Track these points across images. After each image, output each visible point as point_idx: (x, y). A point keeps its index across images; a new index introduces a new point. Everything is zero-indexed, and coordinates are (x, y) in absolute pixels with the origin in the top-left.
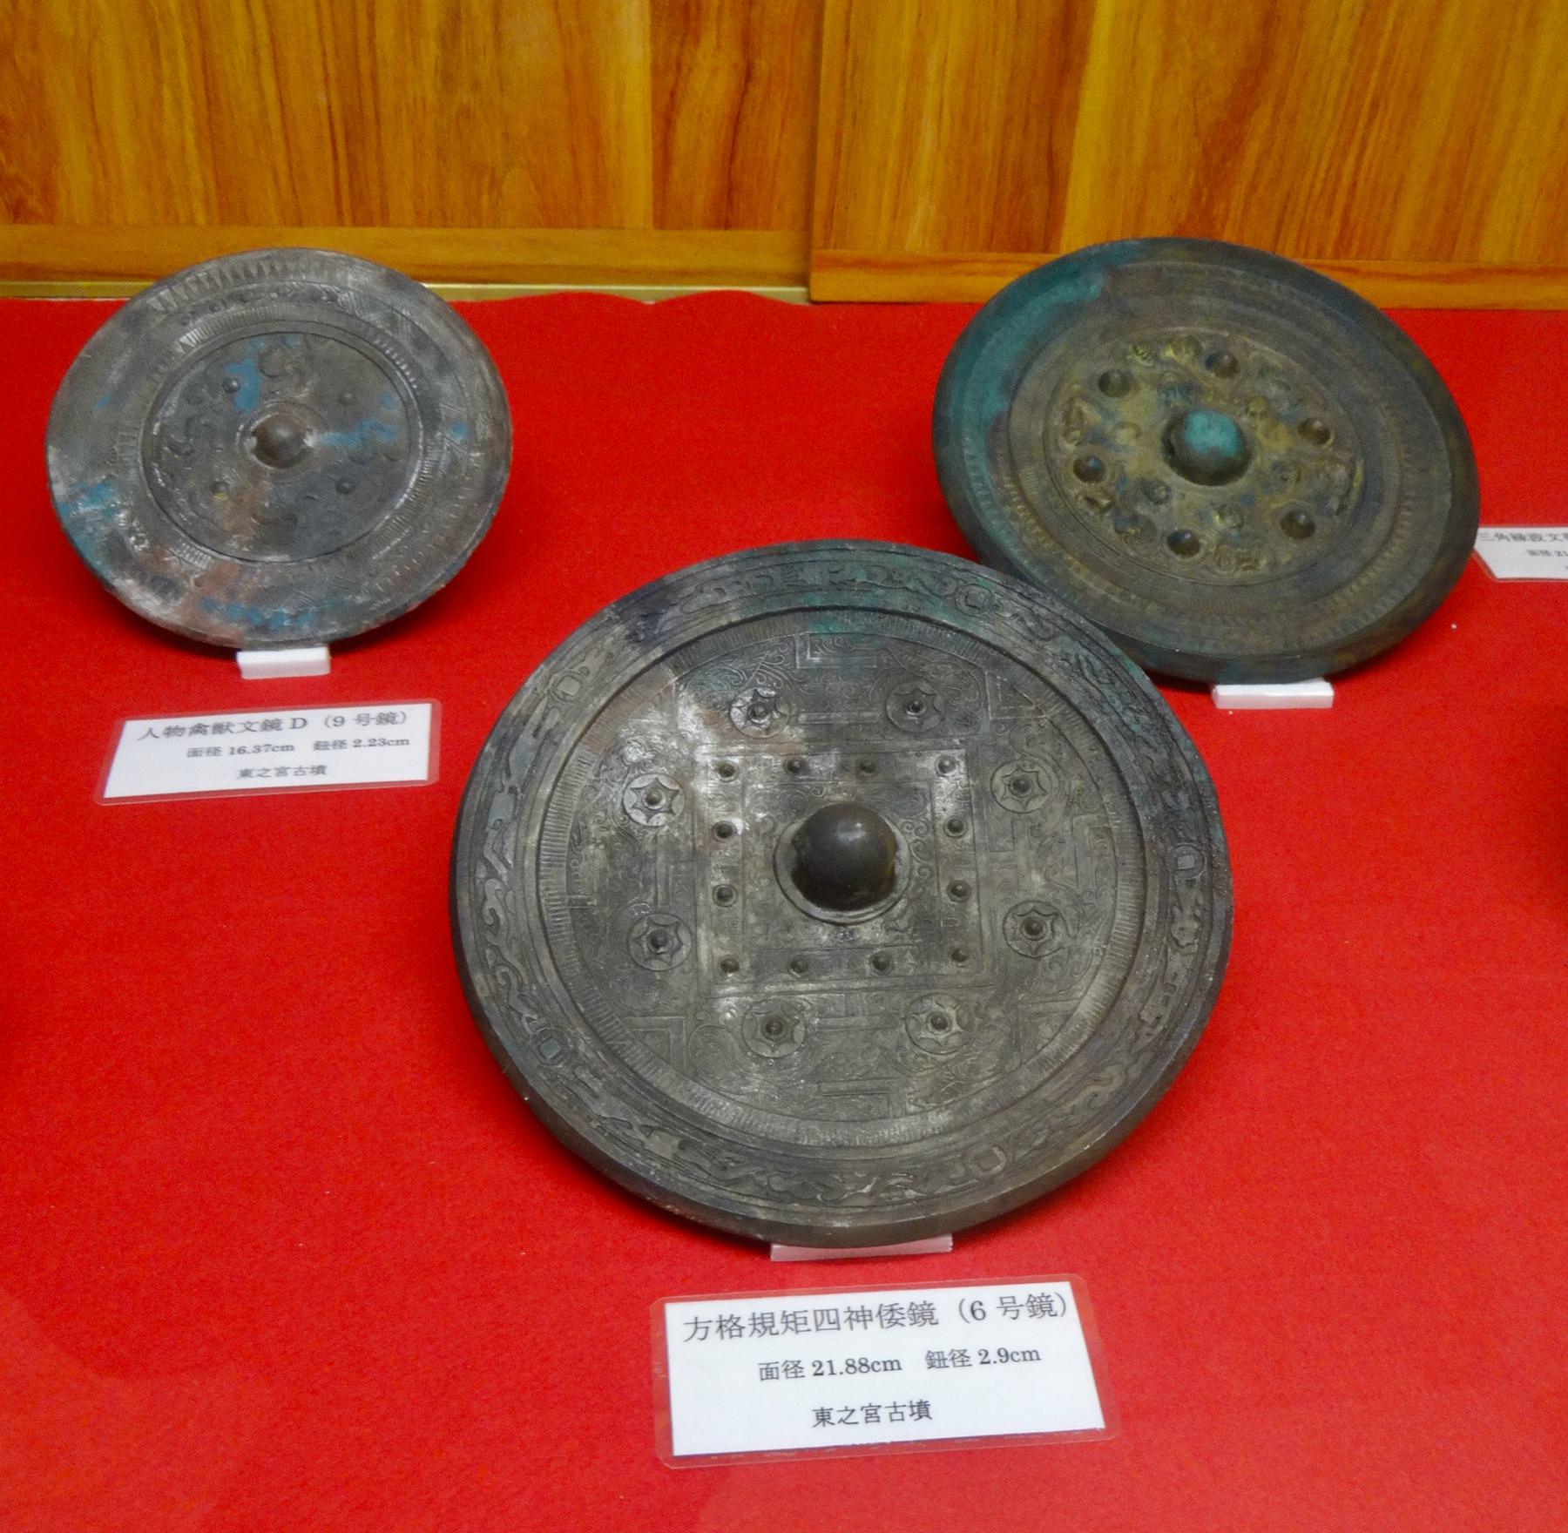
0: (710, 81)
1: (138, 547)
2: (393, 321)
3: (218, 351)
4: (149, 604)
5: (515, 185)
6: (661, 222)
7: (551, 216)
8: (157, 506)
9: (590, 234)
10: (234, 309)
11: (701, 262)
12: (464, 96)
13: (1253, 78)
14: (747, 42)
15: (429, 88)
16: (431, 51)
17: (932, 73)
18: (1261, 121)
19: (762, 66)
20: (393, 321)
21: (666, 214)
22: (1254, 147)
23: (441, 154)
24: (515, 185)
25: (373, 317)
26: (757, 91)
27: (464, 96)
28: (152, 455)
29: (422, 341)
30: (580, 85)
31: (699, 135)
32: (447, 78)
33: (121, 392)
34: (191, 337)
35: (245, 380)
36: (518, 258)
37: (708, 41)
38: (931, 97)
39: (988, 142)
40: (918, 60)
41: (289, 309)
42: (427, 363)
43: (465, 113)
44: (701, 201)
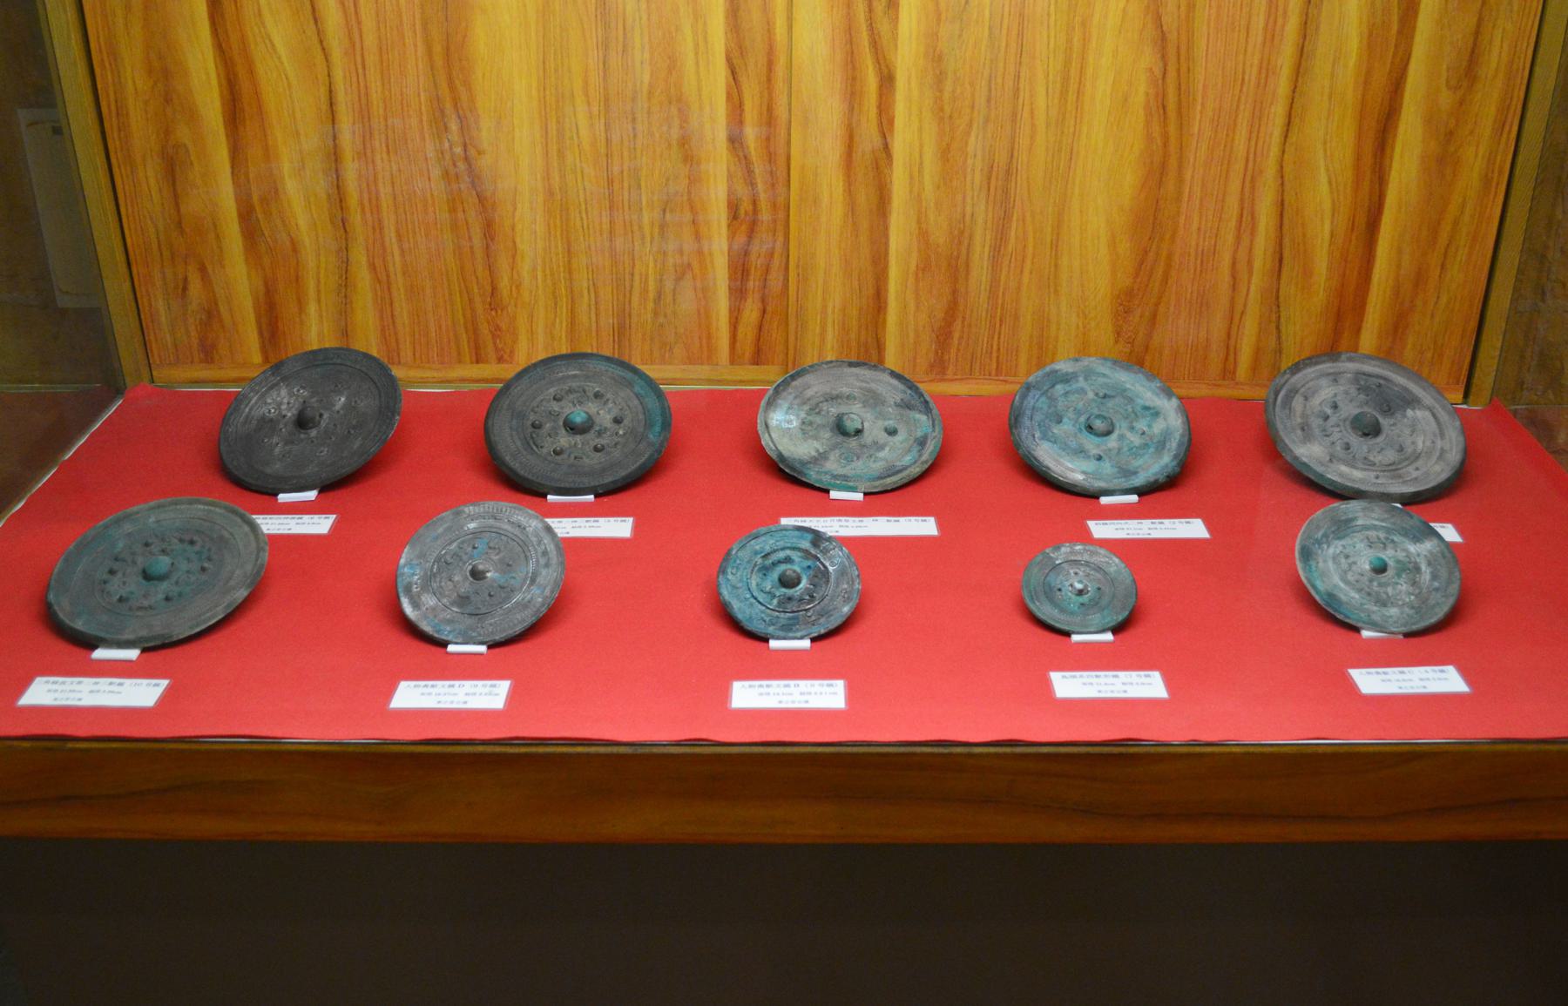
0: (751, 313)
1: (415, 589)
2: (540, 542)
3: (476, 534)
4: (408, 610)
5: (679, 351)
6: (732, 362)
7: (691, 360)
8: (427, 582)
9: (706, 367)
10: (492, 522)
11: (749, 377)
12: (661, 320)
13: (952, 310)
14: (763, 300)
15: (649, 316)
16: (650, 305)
17: (830, 311)
18: (957, 326)
19: (769, 309)
20: (540, 542)
21: (734, 359)
22: (956, 335)
23: (652, 339)
24: (679, 351)
25: (534, 539)
26: (768, 317)
27: (661, 320)
28: (438, 560)
29: (545, 553)
30: (704, 315)
31: (747, 332)
32: (656, 314)
33: (437, 538)
34: (472, 526)
35: (481, 545)
36: (678, 376)
37: (750, 300)
38: (830, 320)
39: (853, 336)
40: (825, 307)
41: (506, 527)
42: (542, 561)
43: (661, 325)
44: (748, 355)
